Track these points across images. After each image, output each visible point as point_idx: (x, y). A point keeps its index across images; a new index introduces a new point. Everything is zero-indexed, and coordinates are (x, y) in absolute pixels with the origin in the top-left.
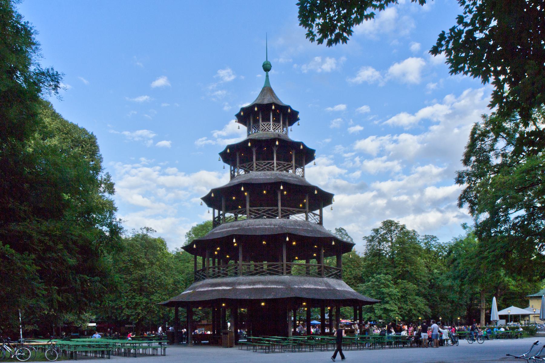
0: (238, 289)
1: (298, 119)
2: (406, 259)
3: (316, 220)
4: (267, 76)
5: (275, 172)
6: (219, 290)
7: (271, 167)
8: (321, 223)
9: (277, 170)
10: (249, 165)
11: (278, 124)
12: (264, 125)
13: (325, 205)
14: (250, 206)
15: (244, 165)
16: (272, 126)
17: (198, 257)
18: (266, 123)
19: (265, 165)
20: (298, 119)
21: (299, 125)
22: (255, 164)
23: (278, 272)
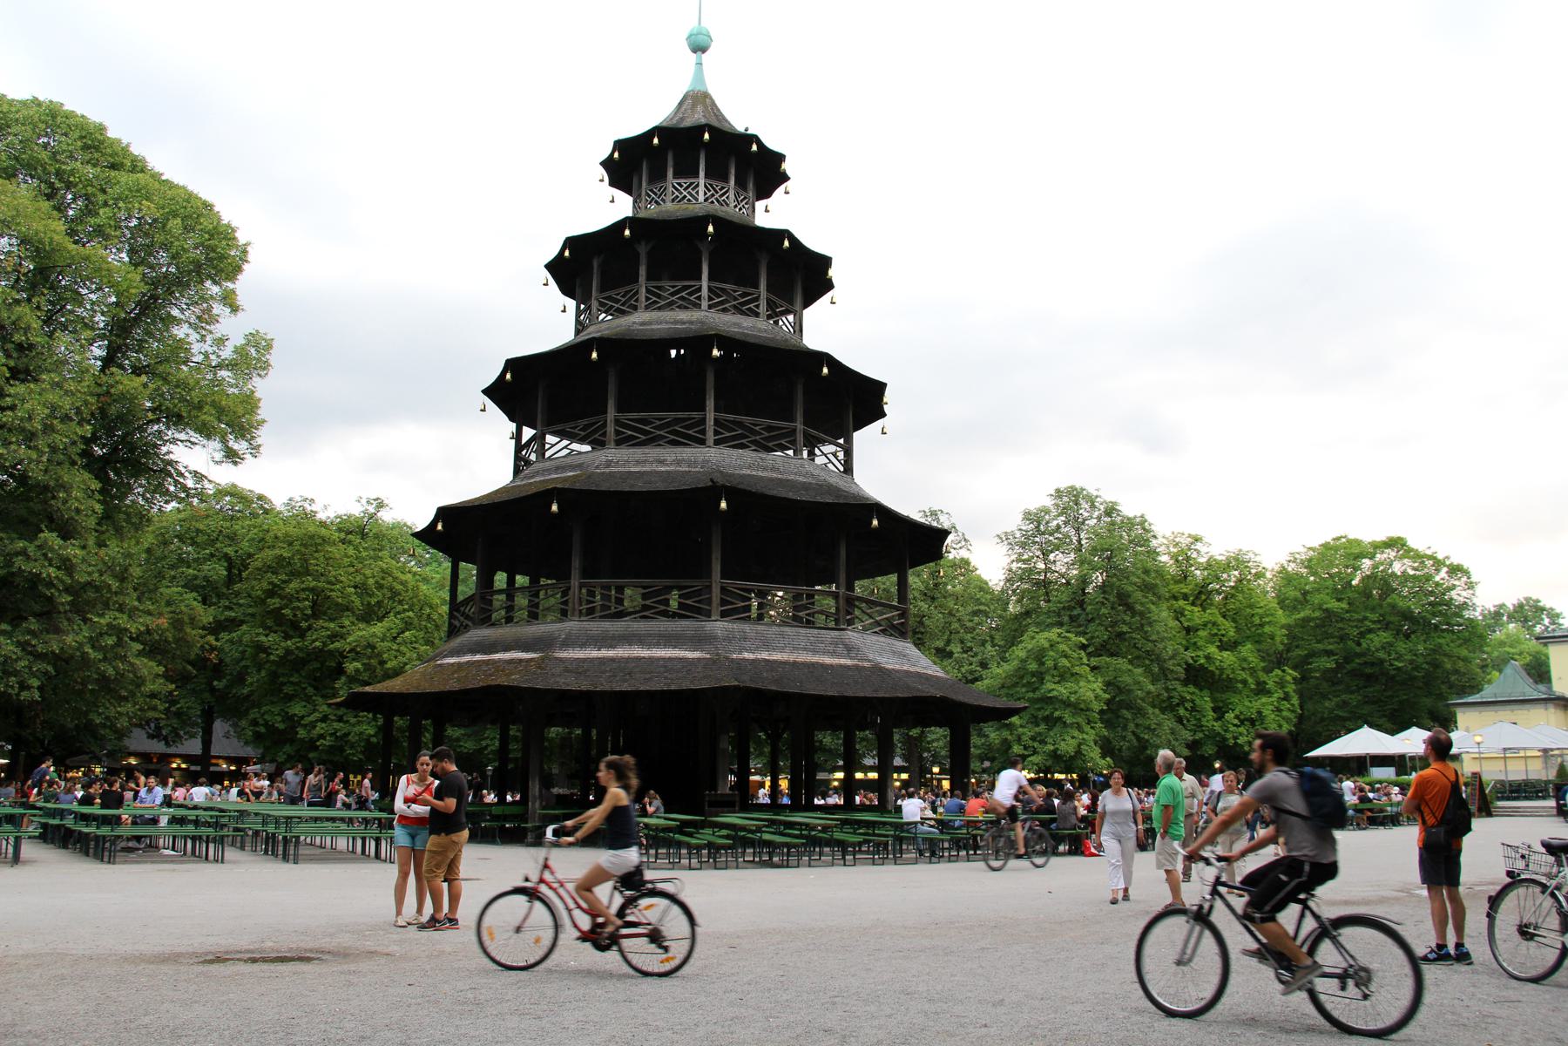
0: (561, 659)
1: (784, 178)
2: (1123, 599)
3: (831, 457)
4: (700, 64)
5: (703, 313)
6: (494, 662)
7: (692, 298)
8: (848, 469)
9: (710, 307)
10: (627, 293)
11: (721, 184)
12: (681, 186)
13: (862, 423)
14: (620, 409)
15: (612, 293)
16: (701, 189)
17: (463, 565)
18: (685, 182)
19: (673, 294)
20: (784, 178)
21: (787, 193)
22: (643, 290)
23: (699, 611)
